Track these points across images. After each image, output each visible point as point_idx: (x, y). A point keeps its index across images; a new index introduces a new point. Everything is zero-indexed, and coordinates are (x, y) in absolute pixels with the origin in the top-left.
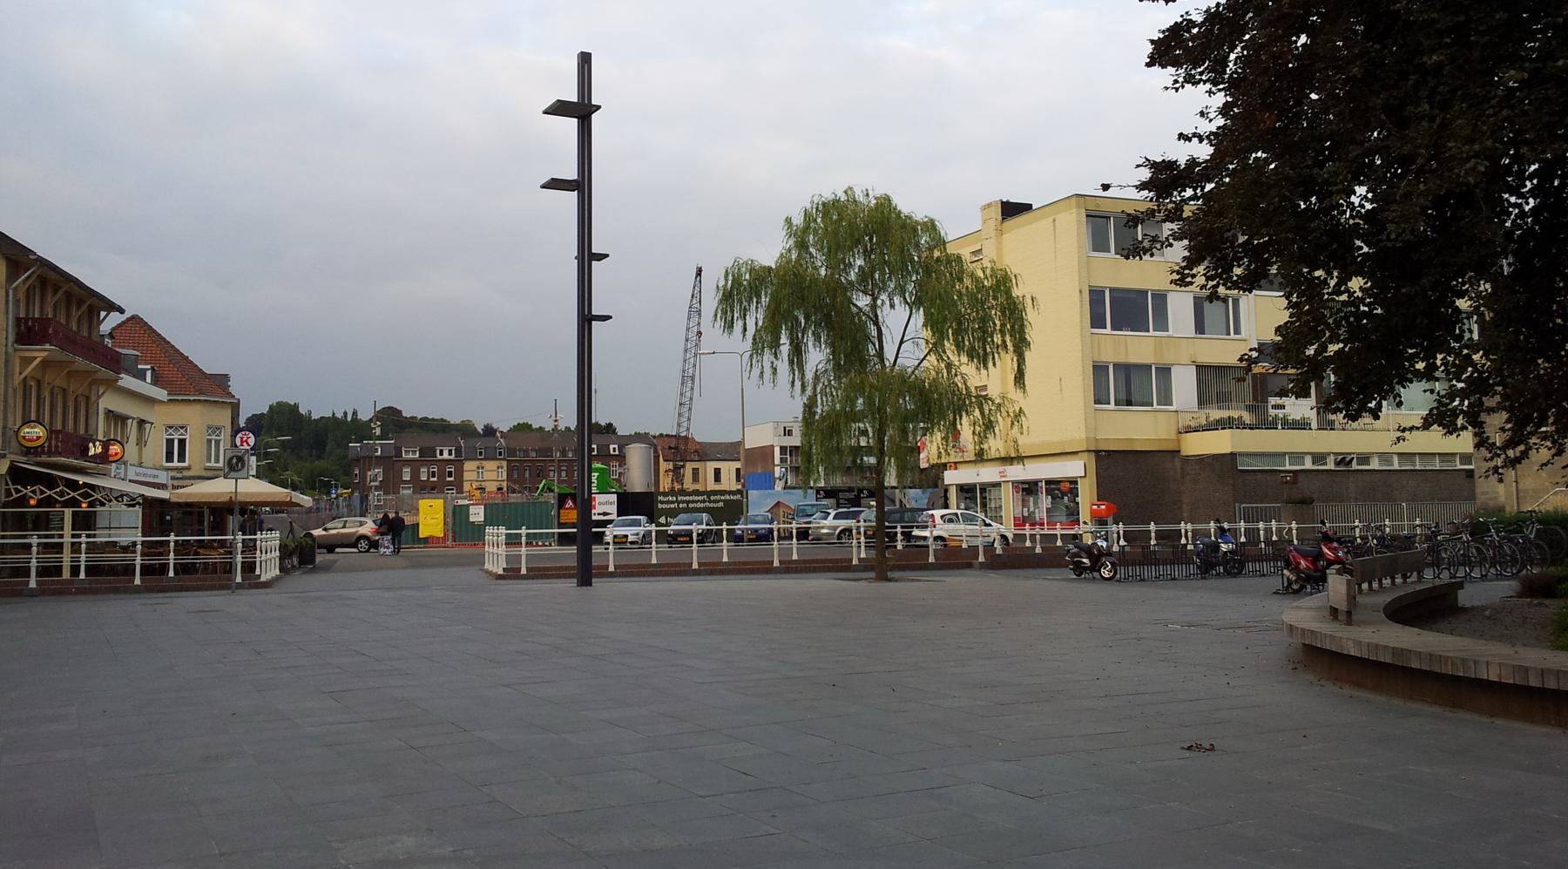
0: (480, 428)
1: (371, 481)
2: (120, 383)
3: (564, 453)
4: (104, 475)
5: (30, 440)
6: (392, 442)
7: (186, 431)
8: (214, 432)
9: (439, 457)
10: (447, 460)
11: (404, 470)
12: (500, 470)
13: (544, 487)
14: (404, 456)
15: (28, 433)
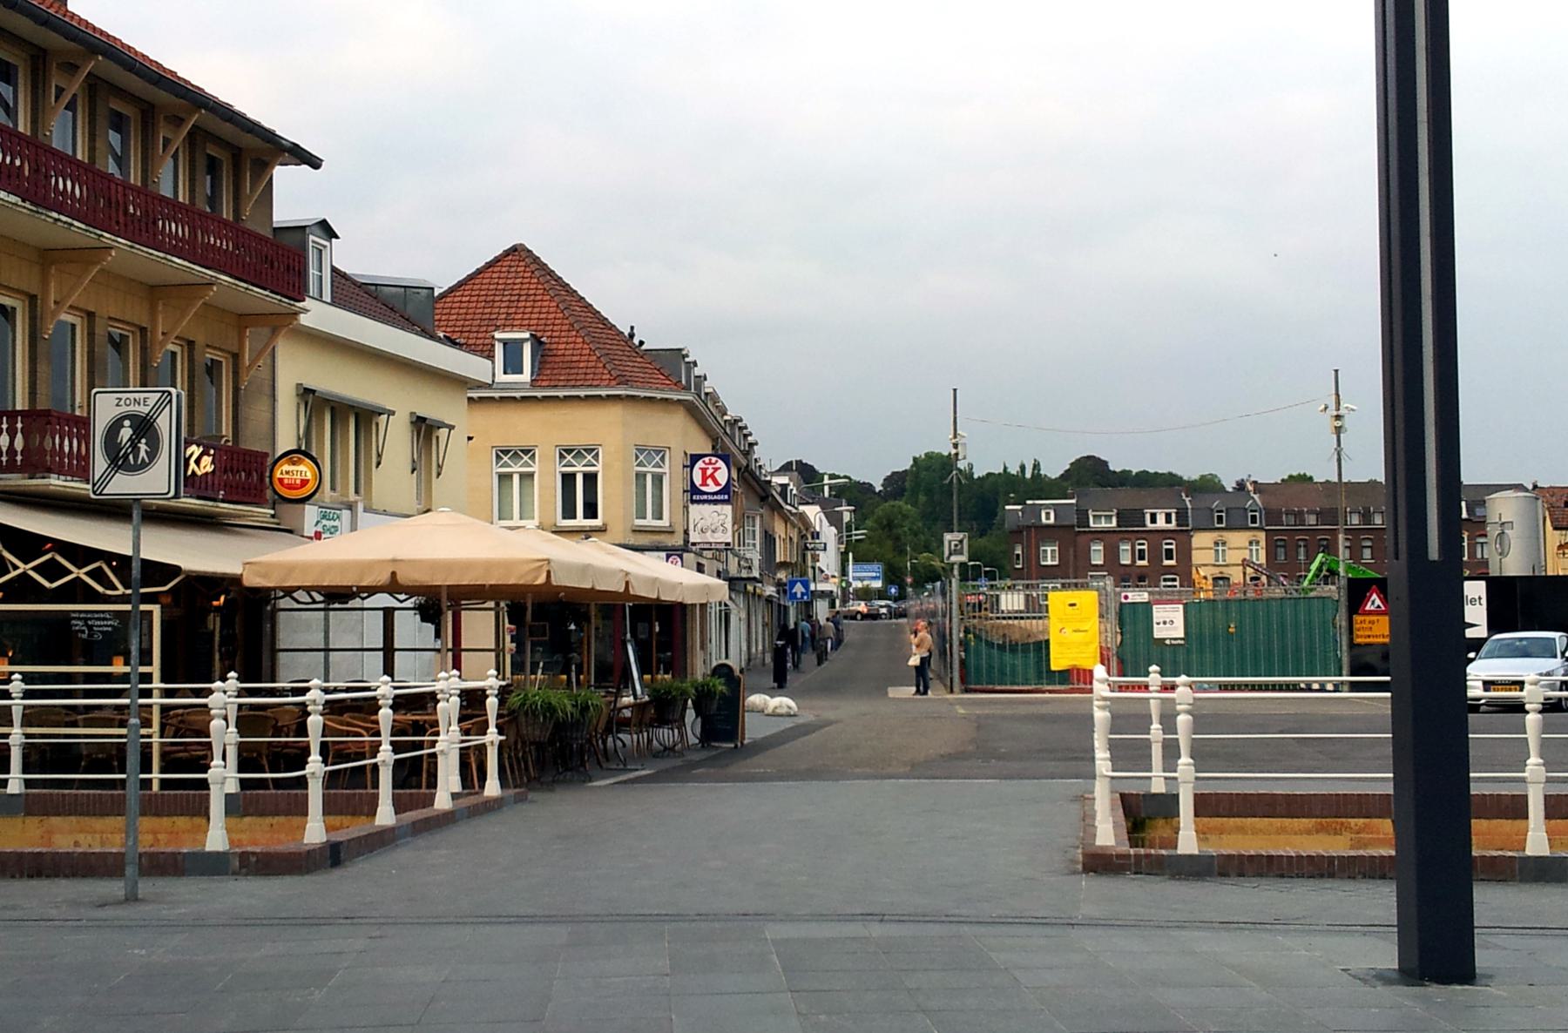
0: (1229, 486)
1: (950, 554)
2: (304, 320)
3: (1366, 516)
4: (290, 531)
5: (291, 487)
6: (1073, 501)
7: (596, 457)
8: (650, 458)
9: (1150, 526)
10: (1163, 531)
11: (1093, 548)
12: (1254, 548)
13: (1320, 569)
14: (1091, 524)
15: (287, 473)
